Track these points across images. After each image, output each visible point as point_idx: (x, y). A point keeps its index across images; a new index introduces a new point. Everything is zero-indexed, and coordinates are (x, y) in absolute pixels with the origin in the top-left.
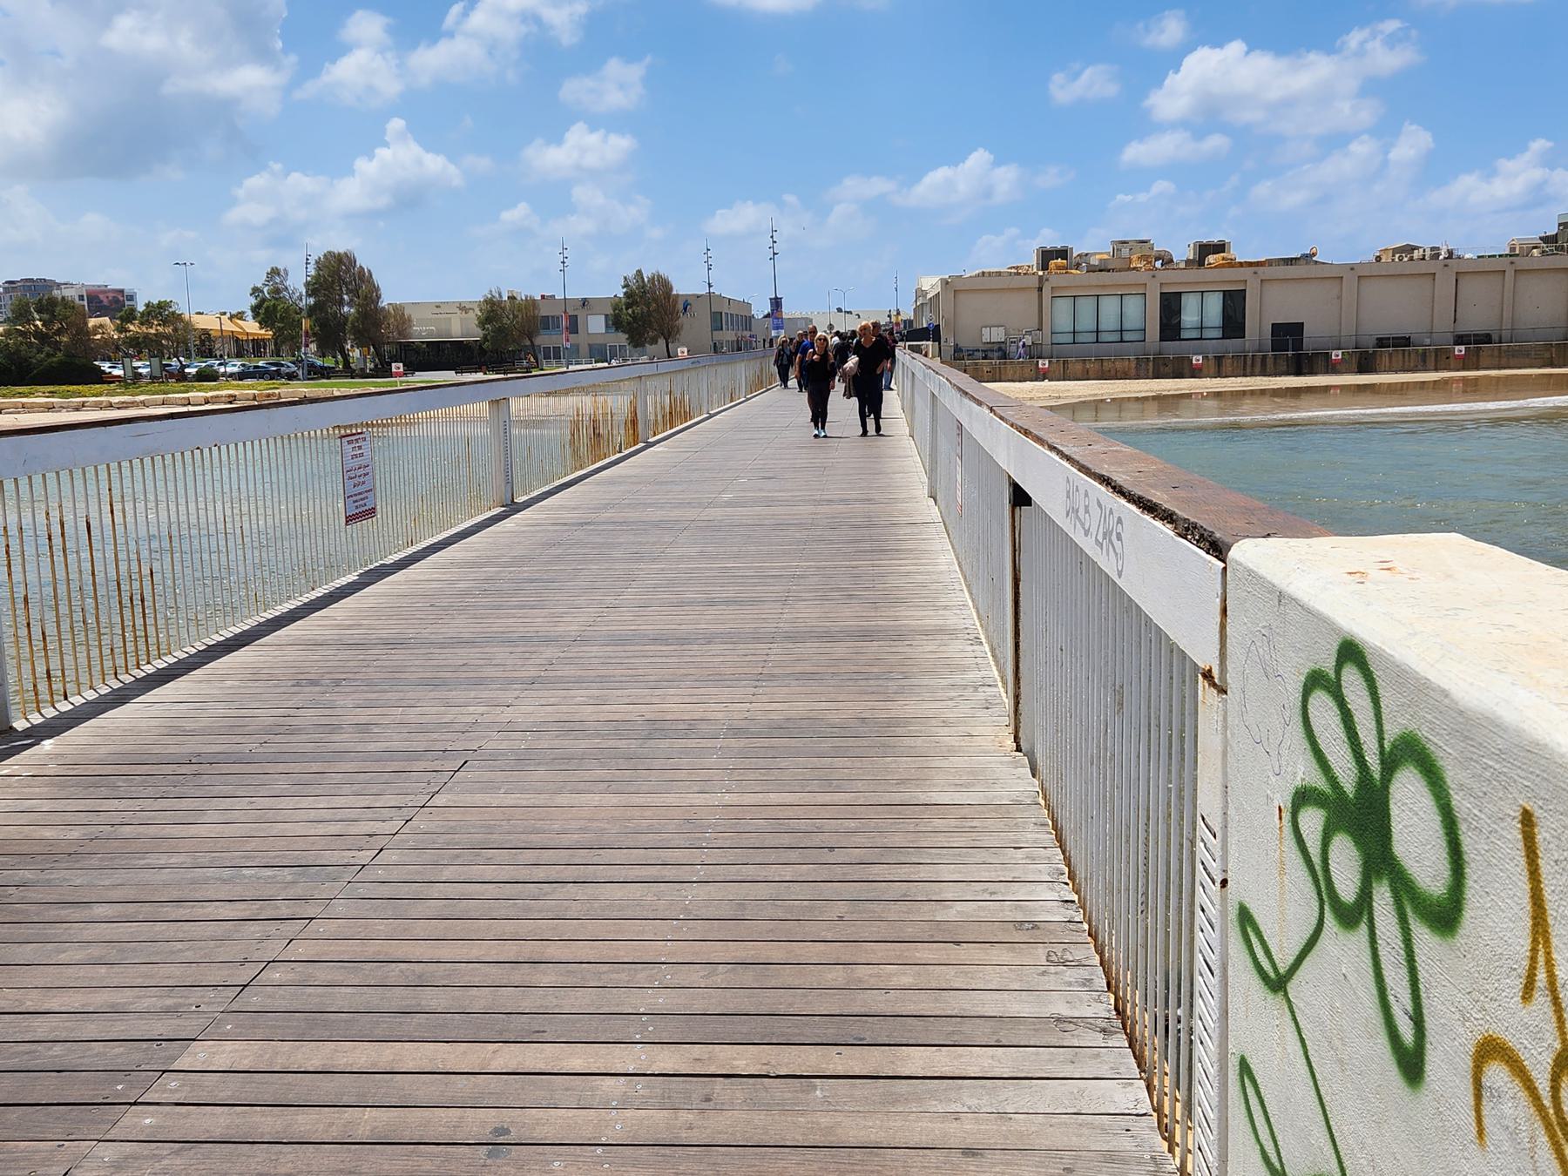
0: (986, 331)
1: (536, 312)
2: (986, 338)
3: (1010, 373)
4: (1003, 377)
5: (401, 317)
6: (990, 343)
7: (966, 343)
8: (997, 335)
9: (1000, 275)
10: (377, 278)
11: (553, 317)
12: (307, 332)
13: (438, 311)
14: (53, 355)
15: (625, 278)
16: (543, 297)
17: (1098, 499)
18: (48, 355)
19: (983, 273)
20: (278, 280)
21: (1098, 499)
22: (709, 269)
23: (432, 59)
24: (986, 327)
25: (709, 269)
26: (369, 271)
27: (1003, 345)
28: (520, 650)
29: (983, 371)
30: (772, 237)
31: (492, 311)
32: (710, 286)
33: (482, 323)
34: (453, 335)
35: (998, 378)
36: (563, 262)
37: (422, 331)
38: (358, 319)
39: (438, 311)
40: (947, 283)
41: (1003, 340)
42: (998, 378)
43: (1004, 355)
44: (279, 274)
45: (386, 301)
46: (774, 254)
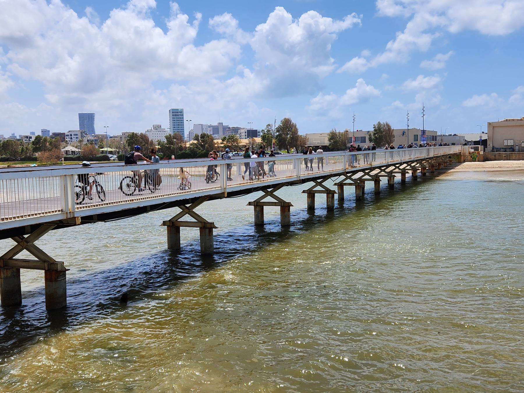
0: (505, 141)
1: (348, 136)
2: (506, 144)
3: (514, 157)
4: (511, 159)
5: (304, 140)
6: (507, 146)
7: (497, 146)
8: (510, 143)
9: (514, 121)
10: (297, 127)
11: (358, 137)
12: (274, 143)
13: (321, 136)
14: (203, 151)
15: (374, 125)
16: (357, 131)
17: (70, 270)
18: (202, 151)
19: (507, 120)
20: (270, 127)
21: (70, 270)
22: (408, 120)
23: (383, 58)
24: (506, 140)
25: (408, 120)
26: (295, 124)
27: (513, 147)
28: (73, 306)
29: (503, 156)
30: (423, 109)
31: (333, 136)
32: (408, 126)
33: (330, 140)
34: (325, 143)
35: (509, 159)
36: (354, 120)
37: (314, 142)
38: (290, 139)
39: (321, 136)
40: (490, 124)
41: (513, 145)
42: (509, 159)
43: (513, 150)
44: (270, 125)
45: (300, 133)
46: (424, 115)
